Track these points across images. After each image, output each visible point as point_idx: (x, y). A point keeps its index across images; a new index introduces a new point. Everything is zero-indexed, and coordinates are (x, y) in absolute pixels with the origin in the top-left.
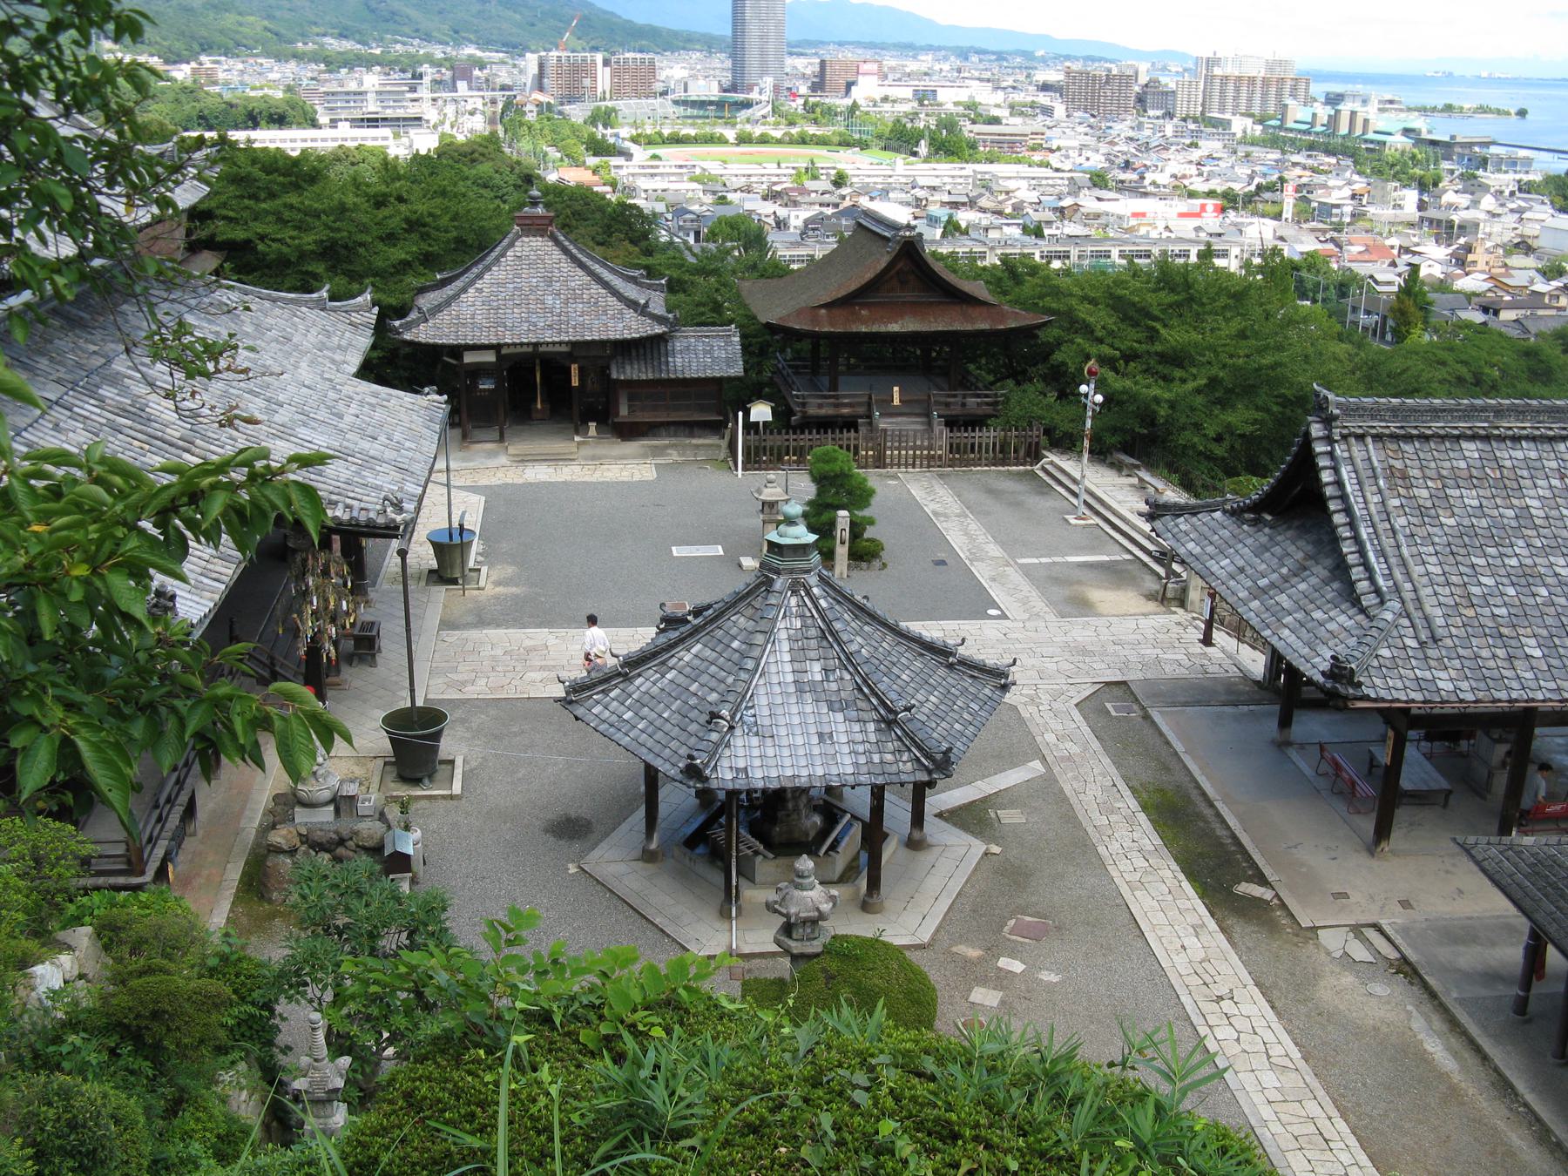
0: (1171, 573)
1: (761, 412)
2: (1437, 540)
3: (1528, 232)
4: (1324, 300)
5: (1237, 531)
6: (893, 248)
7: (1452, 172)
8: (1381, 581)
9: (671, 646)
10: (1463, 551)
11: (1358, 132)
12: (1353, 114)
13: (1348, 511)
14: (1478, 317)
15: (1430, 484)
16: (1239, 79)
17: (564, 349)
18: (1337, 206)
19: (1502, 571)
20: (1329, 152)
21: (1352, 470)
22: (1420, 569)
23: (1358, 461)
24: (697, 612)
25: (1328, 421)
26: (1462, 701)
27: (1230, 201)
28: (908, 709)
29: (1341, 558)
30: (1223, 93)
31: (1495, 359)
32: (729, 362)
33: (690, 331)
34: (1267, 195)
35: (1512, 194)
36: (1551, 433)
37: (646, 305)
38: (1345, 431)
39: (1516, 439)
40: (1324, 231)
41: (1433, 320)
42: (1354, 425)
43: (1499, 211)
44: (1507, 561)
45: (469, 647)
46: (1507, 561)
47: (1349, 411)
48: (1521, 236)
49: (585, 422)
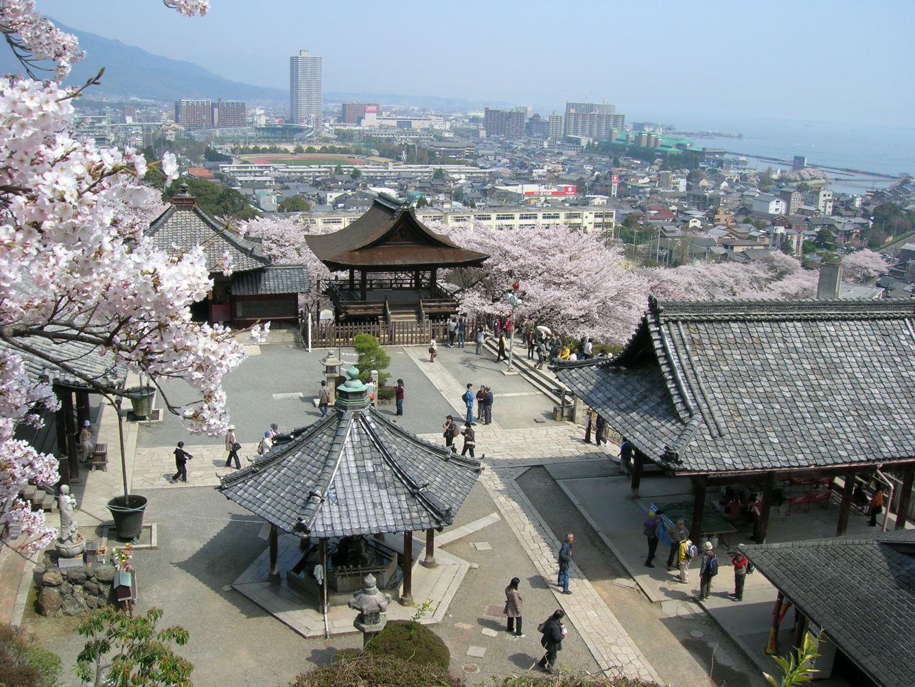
0: (564, 401)
5: (606, 376)
6: (397, 216)
8: (690, 403)
9: (284, 453)
10: (734, 385)
12: (649, 135)
13: (670, 364)
15: (714, 347)
18: (642, 188)
24: (297, 433)
26: (737, 469)
28: (425, 486)
29: (667, 390)
30: (576, 124)
35: (737, 181)
36: (777, 317)
37: (252, 251)
38: (666, 319)
39: (759, 321)
43: (730, 190)
45: (156, 457)
46: (757, 389)
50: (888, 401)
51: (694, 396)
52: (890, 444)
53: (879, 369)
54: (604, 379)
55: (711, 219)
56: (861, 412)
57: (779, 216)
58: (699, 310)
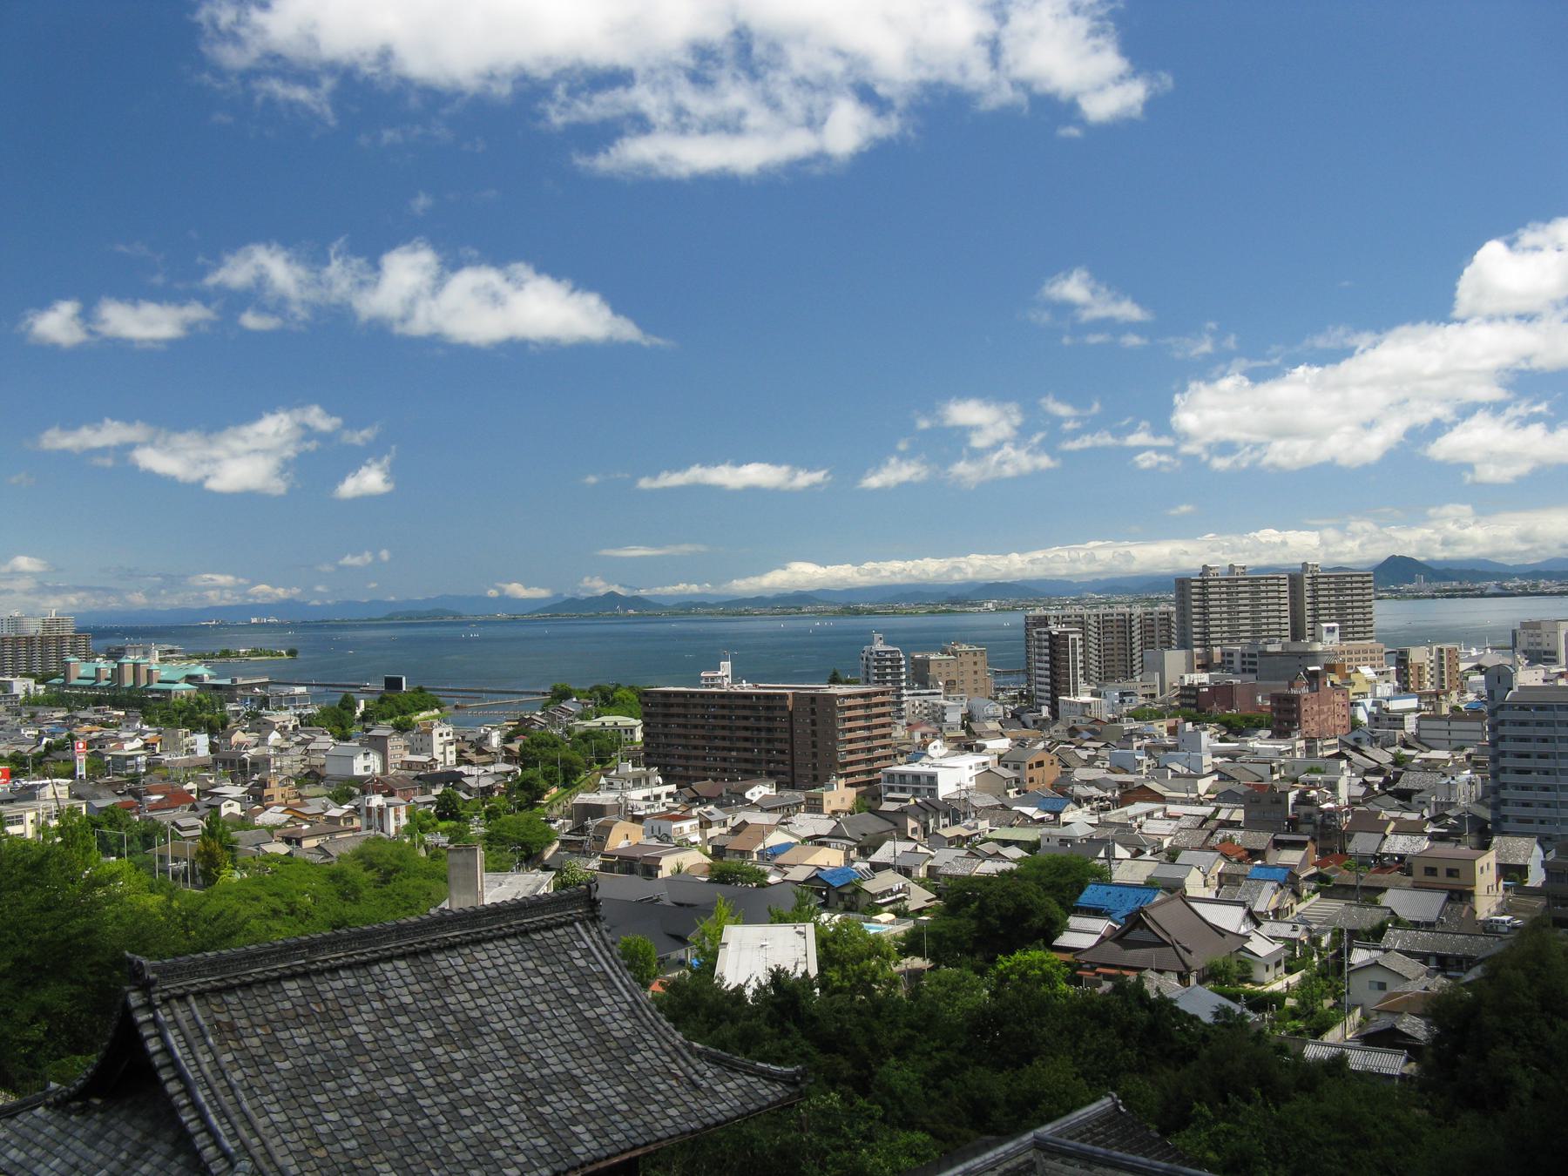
2: (276, 1086)
3: (315, 762)
4: (129, 853)
5: (64, 1125)
7: (237, 713)
8: (227, 1144)
10: (303, 1092)
11: (143, 683)
13: (181, 1076)
14: (282, 849)
15: (259, 1031)
16: (16, 640)
18: (131, 758)
19: (345, 1103)
20: (116, 706)
21: (177, 1034)
22: (264, 1121)
25: (146, 987)
27: (19, 764)
29: (183, 1127)
34: (58, 754)
35: (295, 727)
38: (165, 995)
39: (333, 970)
40: (121, 783)
41: (240, 858)
42: (174, 987)
43: (286, 745)
44: (347, 1092)
46: (347, 1092)
47: (165, 973)
48: (310, 766)
50: (571, 1065)
51: (233, 1127)
52: (587, 1137)
53: (547, 1014)
54: (62, 1131)
55: (258, 796)
56: (530, 1094)
57: (372, 778)
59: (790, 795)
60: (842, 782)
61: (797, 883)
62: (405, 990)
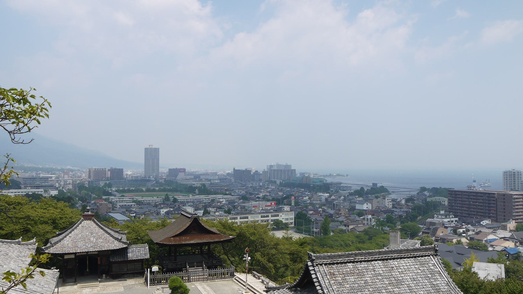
1: (155, 268)
13: (320, 286)
17: (96, 253)
20: (302, 188)
23: (321, 271)
25: (312, 261)
31: (350, 238)
32: (145, 254)
33: (134, 246)
37: (121, 239)
39: (361, 262)
42: (318, 261)
47: (317, 258)
49: (102, 275)
58: (332, 258)
59: (496, 224)
60: (514, 221)
61: (498, 251)
62: (380, 270)
